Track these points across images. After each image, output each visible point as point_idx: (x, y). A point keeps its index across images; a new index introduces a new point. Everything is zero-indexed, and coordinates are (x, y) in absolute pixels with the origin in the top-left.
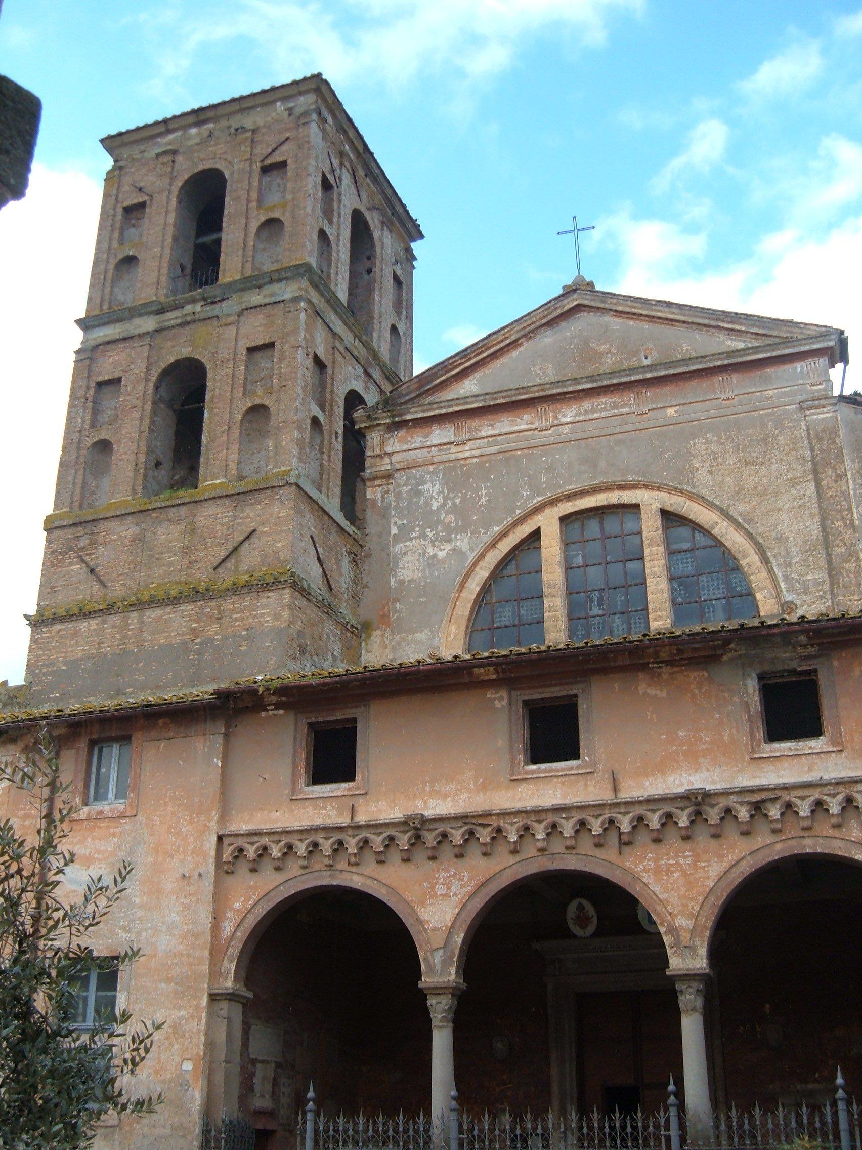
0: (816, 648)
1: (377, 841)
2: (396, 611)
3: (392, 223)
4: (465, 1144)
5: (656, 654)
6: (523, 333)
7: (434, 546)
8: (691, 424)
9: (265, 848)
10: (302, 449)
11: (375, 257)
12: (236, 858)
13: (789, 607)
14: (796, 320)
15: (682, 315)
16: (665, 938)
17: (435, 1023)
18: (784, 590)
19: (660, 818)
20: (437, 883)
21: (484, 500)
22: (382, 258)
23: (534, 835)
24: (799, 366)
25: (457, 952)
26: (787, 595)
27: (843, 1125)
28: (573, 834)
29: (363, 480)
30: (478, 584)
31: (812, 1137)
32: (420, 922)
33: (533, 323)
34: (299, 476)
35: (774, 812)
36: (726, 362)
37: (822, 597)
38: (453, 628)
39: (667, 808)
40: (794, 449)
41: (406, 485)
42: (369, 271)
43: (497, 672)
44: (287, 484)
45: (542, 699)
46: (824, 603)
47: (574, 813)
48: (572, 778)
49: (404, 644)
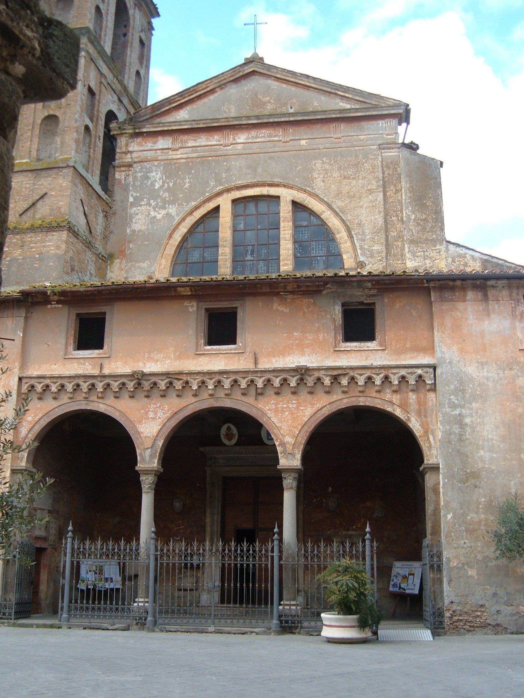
0: (376, 291)
1: (115, 385)
2: (130, 249)
3: (141, 6)
4: (159, 557)
5: (285, 287)
6: (218, 84)
7: (155, 211)
8: (314, 151)
9: (48, 386)
10: (78, 146)
11: (129, 26)
12: (29, 391)
13: (361, 265)
14: (382, 95)
15: (315, 84)
16: (278, 448)
17: (144, 490)
18: (359, 254)
19: (280, 381)
20: (149, 411)
21: (187, 185)
22: (134, 28)
23: (207, 386)
24: (381, 123)
25: (159, 451)
26: (361, 257)
27: (368, 553)
28: (230, 387)
29: (114, 167)
30: (180, 236)
31: (351, 558)
32: (139, 433)
33: (225, 79)
34: (75, 162)
35: (344, 381)
36: (338, 116)
37: (380, 260)
38: (163, 261)
39: (284, 376)
40: (373, 172)
41: (140, 172)
42: (125, 35)
43: (191, 291)
44: (68, 166)
45: (216, 308)
46: (382, 264)
47: (231, 375)
48: (232, 355)
49: (133, 269)
